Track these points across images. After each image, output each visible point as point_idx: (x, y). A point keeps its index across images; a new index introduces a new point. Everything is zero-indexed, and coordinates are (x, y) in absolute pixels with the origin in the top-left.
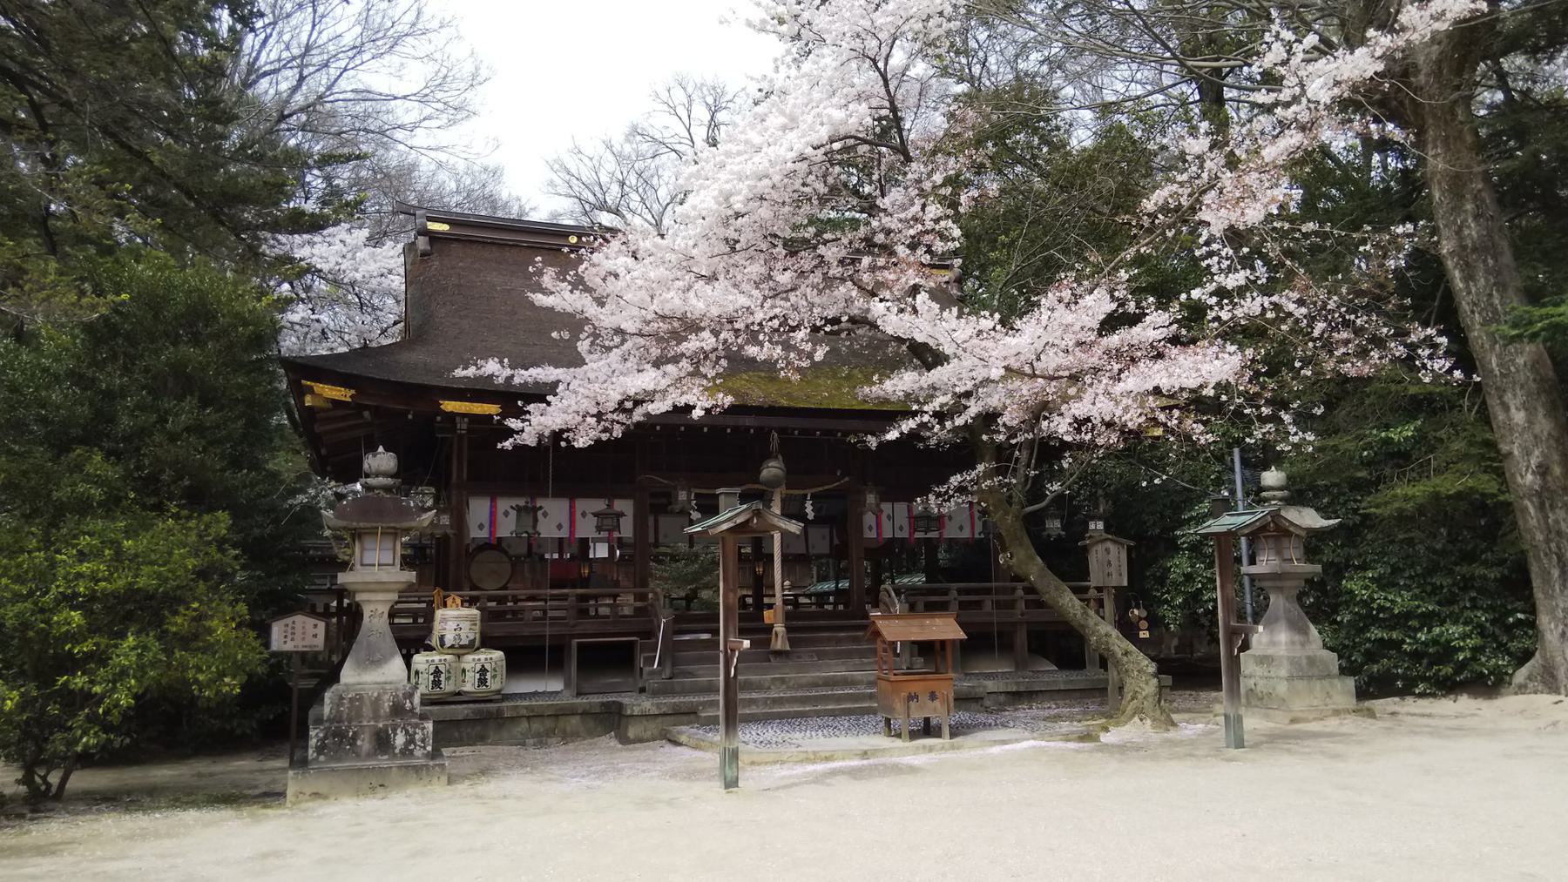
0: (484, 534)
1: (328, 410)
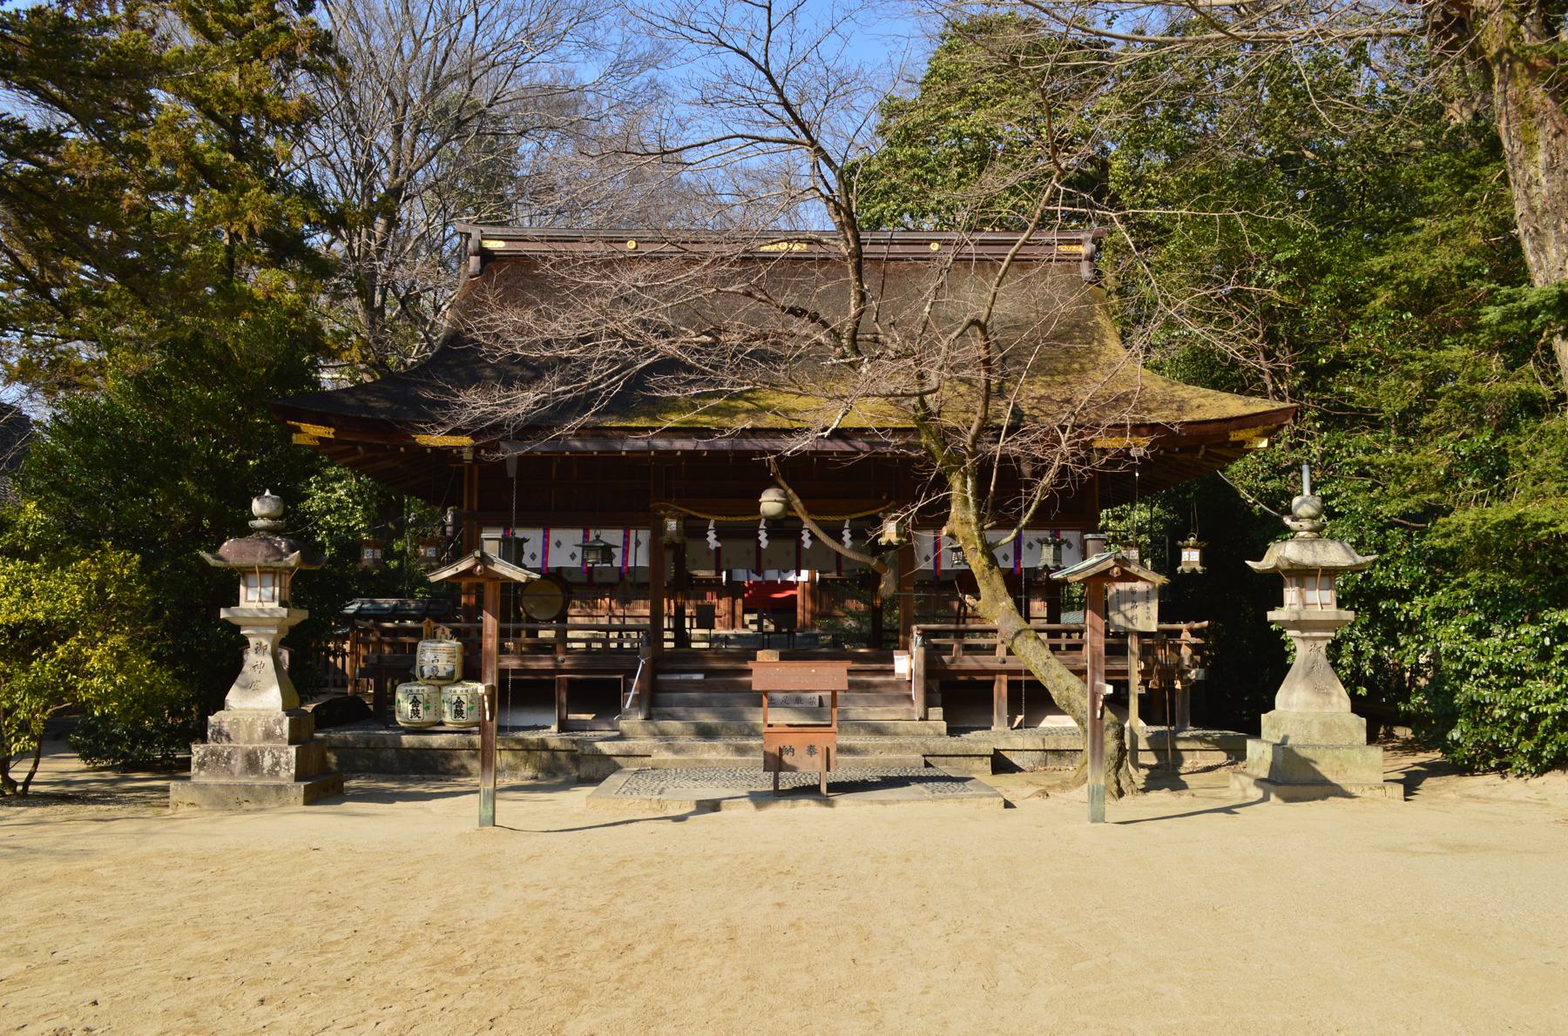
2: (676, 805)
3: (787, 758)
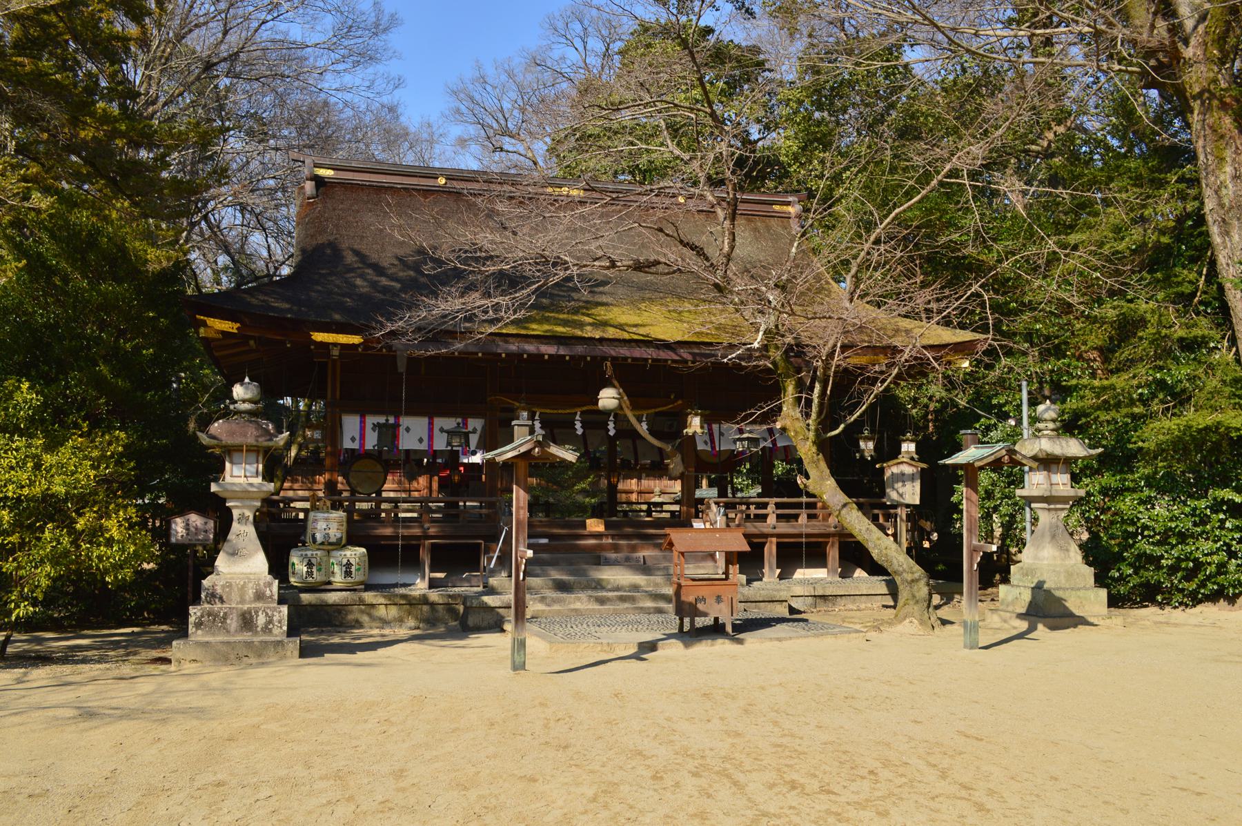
0: (356, 446)
1: (218, 340)
2: (622, 647)
3: (700, 606)
